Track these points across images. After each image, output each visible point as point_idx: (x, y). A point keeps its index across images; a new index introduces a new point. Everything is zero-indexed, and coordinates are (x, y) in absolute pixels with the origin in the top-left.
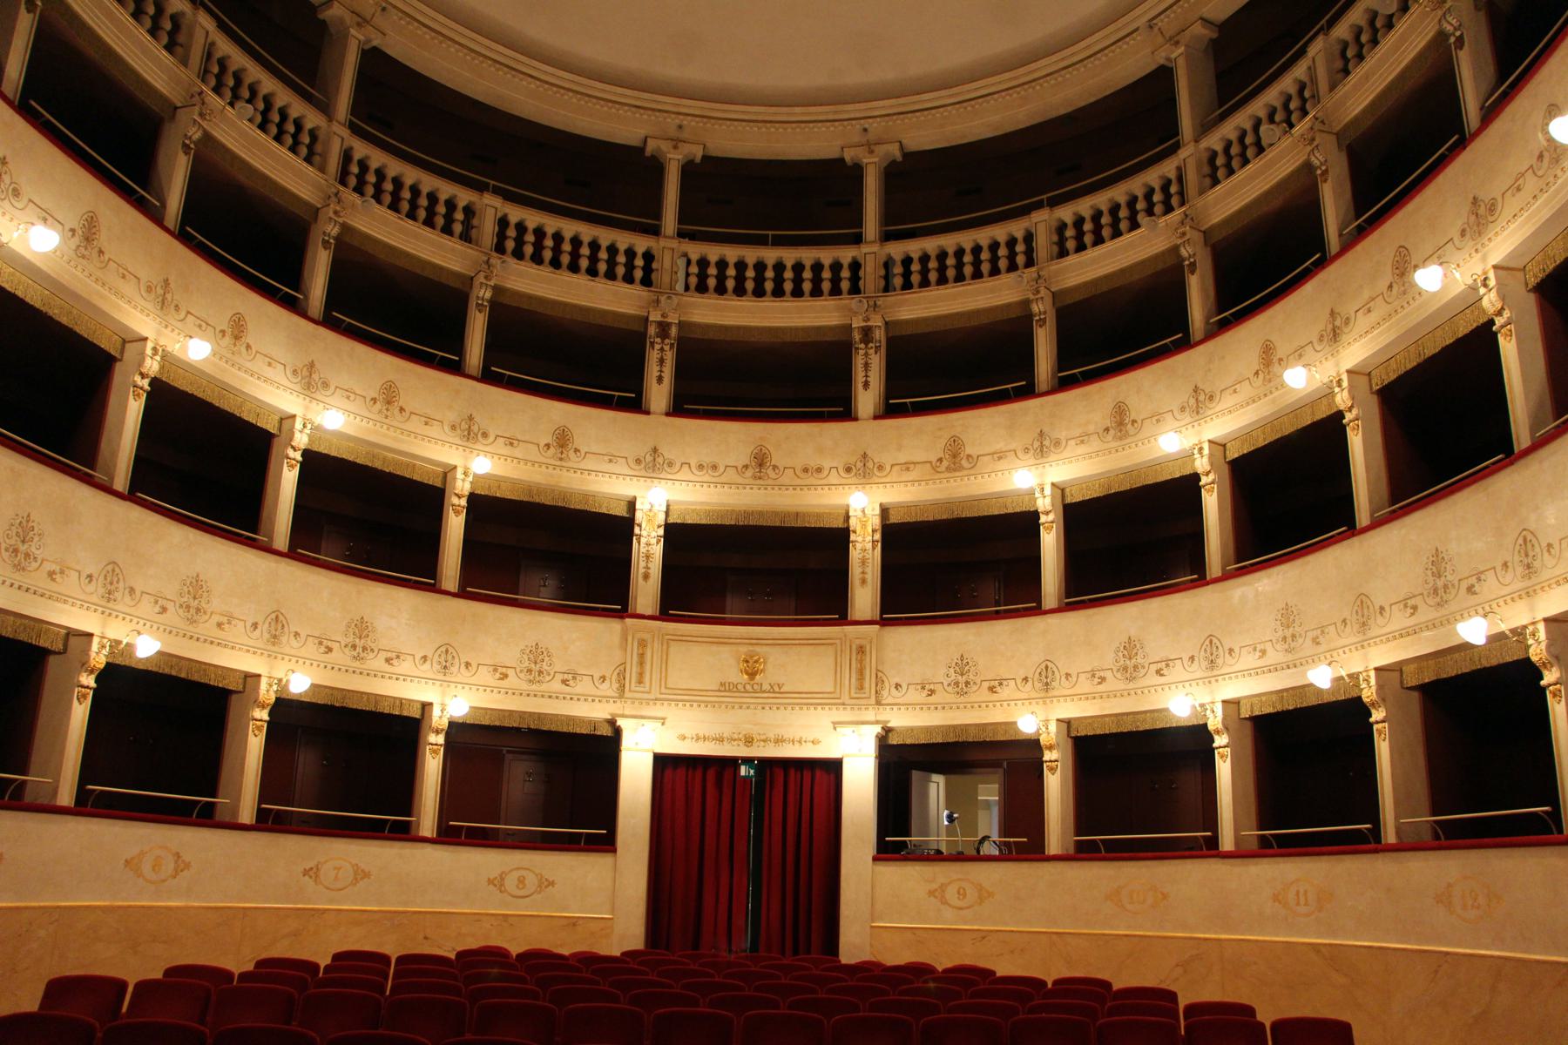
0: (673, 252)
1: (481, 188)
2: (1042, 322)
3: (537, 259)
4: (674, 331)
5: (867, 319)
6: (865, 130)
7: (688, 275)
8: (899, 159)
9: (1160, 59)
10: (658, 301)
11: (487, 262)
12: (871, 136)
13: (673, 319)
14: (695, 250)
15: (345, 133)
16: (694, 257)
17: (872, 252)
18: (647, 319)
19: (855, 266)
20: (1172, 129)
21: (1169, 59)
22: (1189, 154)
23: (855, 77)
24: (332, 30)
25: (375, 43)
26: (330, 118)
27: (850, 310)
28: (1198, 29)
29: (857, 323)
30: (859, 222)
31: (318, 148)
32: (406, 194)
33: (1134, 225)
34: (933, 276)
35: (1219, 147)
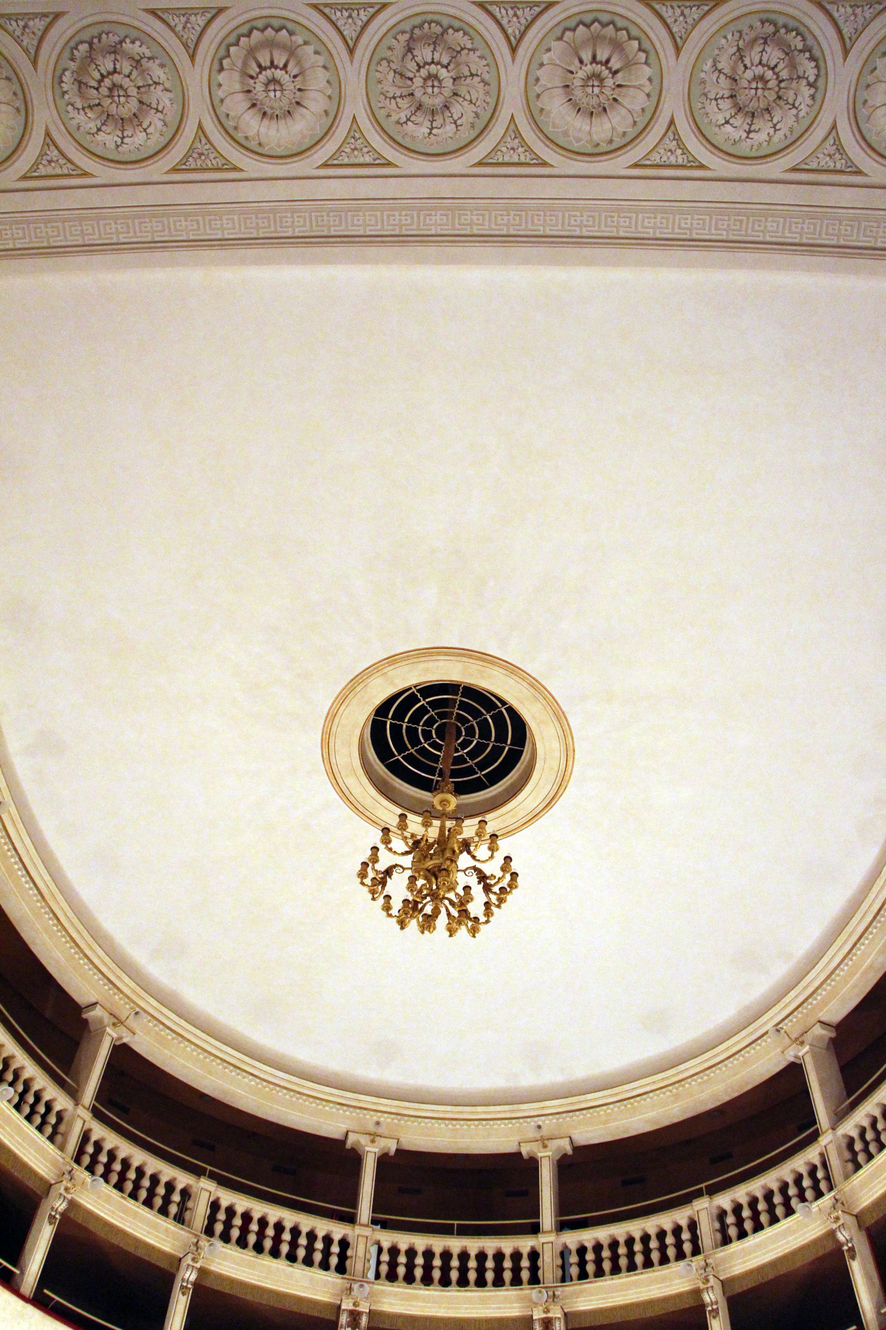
0: (366, 1238)
1: (198, 1172)
2: (715, 1312)
3: (242, 1243)
4: (364, 1320)
5: (547, 1311)
6: (539, 1127)
7: (379, 1263)
8: (570, 1152)
9: (790, 1056)
10: (351, 1289)
11: (196, 1244)
12: (545, 1132)
13: (364, 1308)
14: (387, 1238)
15: (87, 1116)
16: (386, 1245)
17: (549, 1241)
18: (339, 1307)
19: (534, 1255)
20: (811, 1119)
21: (797, 1057)
22: (828, 1143)
23: (528, 1080)
24: (92, 1028)
25: (125, 1040)
26: (77, 1101)
27: (531, 1300)
28: (818, 1030)
29: (538, 1314)
30: (535, 1212)
31: (62, 1128)
32: (132, 1175)
33: (790, 1212)
34: (607, 1266)
35: (855, 1134)
